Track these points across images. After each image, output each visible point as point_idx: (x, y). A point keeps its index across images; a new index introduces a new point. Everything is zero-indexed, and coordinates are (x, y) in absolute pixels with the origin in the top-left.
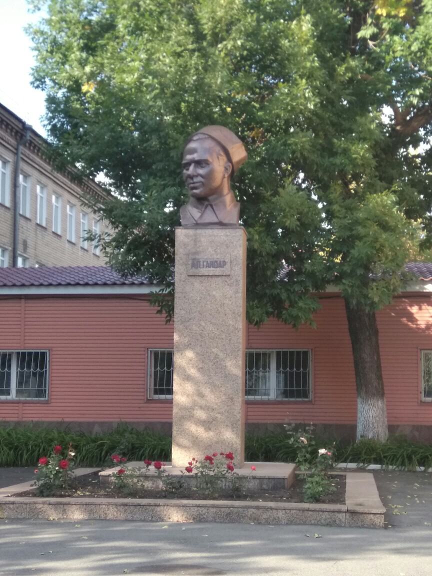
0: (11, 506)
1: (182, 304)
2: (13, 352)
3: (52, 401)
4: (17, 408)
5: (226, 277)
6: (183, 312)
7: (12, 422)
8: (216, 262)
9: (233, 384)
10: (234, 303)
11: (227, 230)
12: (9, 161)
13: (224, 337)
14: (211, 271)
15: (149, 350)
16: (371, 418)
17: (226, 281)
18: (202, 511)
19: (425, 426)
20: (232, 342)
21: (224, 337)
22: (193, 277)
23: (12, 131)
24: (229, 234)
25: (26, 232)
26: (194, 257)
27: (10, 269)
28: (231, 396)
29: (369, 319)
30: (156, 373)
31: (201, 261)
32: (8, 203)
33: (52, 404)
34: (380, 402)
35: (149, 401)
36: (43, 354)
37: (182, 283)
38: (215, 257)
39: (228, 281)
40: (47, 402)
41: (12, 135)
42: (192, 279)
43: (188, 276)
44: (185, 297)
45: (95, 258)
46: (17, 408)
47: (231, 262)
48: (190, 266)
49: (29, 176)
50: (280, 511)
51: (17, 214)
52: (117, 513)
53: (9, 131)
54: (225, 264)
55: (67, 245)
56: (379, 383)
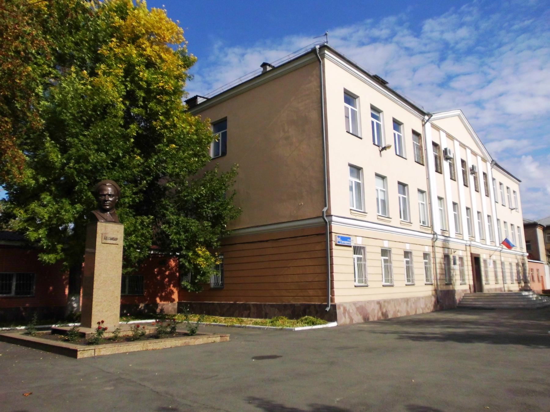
0: (104, 349)
14: (112, 242)
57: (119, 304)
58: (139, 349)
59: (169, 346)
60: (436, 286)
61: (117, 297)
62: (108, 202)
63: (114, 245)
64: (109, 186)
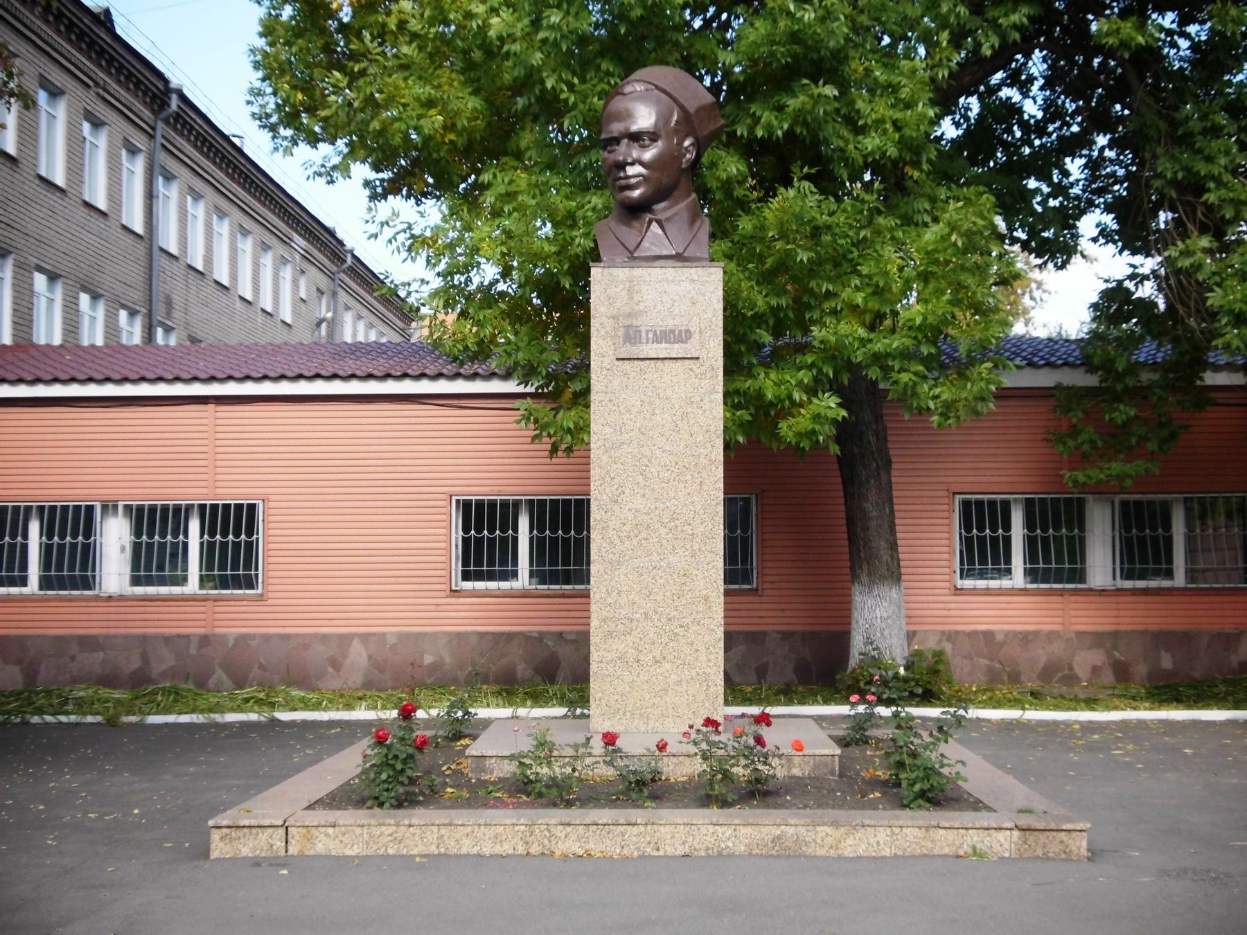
0: (330, 831)
2: (193, 505)
3: (270, 595)
4: (203, 609)
5: (692, 362)
6: (607, 430)
7: (195, 635)
8: (673, 331)
10: (708, 412)
11: (693, 270)
12: (141, 150)
14: (662, 350)
15: (454, 498)
16: (879, 621)
18: (724, 833)
19: (963, 632)
20: (705, 488)
21: (689, 477)
22: (627, 362)
23: (145, 94)
24: (695, 277)
25: (171, 282)
26: (628, 322)
27: (141, 348)
28: (704, 592)
29: (877, 439)
30: (466, 541)
31: (643, 329)
32: (139, 227)
33: (270, 602)
34: (894, 590)
35: (455, 593)
36: (252, 508)
37: (606, 372)
38: (670, 323)
40: (261, 598)
41: (145, 103)
42: (627, 365)
44: (610, 401)
45: (285, 329)
46: (203, 609)
47: (701, 332)
48: (621, 340)
49: (174, 177)
50: (881, 829)
51: (155, 249)
52: (550, 841)
53: (140, 94)
54: (690, 338)
55: (239, 304)
56: (892, 557)
57: (720, 633)
58: (507, 848)
59: (680, 851)
60: (1210, 522)
61: (706, 598)
62: (631, 170)
63: (679, 363)
64: (642, 98)
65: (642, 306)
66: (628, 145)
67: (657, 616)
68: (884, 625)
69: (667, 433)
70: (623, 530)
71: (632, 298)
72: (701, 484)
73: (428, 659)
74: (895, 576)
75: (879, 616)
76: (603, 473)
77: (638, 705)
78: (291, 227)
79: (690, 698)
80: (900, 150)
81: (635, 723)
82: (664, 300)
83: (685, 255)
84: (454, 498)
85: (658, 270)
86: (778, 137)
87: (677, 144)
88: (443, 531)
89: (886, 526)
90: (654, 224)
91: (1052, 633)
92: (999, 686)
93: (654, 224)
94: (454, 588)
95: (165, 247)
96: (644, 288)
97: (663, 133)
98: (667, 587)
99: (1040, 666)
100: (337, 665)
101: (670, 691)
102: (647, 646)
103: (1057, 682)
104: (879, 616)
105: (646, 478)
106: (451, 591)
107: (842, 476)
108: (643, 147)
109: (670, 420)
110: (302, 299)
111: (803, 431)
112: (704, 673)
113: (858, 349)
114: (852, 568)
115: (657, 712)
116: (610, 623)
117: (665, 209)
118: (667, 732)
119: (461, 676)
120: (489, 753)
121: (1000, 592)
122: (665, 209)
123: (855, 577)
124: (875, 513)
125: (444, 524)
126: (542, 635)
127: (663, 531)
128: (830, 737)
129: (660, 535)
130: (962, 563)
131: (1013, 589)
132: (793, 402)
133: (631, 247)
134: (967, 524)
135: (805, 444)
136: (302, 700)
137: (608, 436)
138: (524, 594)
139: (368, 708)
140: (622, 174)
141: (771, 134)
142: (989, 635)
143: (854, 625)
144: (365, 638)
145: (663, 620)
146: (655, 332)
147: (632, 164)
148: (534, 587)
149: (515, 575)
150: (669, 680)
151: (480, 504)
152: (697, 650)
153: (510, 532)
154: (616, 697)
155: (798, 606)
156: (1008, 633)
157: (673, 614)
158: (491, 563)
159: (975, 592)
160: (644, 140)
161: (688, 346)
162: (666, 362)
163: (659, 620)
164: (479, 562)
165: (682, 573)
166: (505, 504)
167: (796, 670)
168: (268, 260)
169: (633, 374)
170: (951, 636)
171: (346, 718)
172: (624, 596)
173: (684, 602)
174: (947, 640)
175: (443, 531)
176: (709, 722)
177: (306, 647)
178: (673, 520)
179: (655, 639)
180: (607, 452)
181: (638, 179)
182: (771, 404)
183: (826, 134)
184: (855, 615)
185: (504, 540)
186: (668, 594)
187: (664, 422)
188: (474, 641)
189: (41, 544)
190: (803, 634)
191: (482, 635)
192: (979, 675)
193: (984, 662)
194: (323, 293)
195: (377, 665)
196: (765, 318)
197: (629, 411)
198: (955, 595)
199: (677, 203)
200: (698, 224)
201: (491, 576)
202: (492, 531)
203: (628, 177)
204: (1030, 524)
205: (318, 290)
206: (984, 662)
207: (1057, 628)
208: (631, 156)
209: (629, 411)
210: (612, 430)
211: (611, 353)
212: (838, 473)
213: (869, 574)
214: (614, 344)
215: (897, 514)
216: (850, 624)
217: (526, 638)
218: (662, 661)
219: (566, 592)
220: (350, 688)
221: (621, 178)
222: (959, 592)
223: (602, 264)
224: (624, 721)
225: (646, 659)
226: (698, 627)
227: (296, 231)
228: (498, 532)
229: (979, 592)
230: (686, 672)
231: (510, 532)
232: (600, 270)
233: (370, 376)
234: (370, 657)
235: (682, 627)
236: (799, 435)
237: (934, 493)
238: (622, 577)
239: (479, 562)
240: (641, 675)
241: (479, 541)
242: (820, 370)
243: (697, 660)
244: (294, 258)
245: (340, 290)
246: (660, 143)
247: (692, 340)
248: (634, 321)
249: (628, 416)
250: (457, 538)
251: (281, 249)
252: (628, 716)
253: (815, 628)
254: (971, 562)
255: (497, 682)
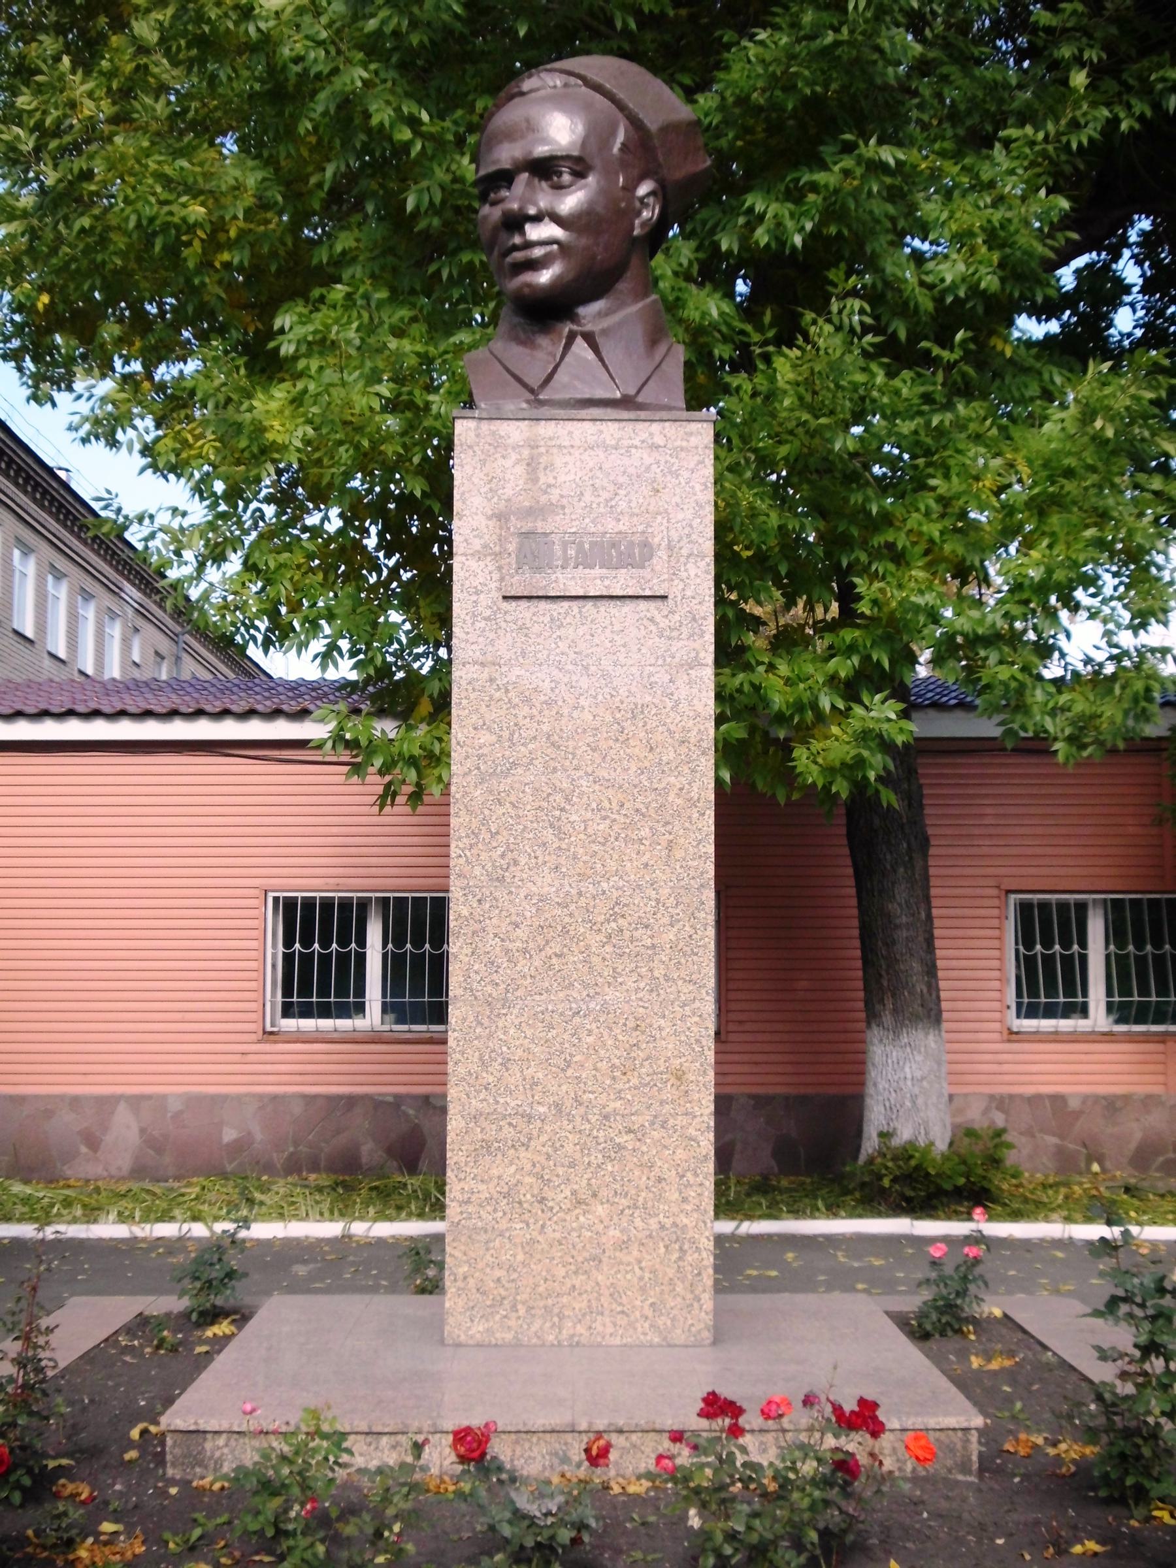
1: (483, 709)
5: (652, 605)
6: (485, 738)
9: (683, 1018)
11: (655, 427)
13: (645, 832)
15: (271, 895)
16: (909, 1083)
17: (652, 620)
19: (1021, 1097)
20: (679, 854)
21: (645, 832)
22: (524, 604)
24: (659, 440)
26: (527, 526)
30: (288, 959)
34: (931, 1037)
35: (270, 1035)
39: (658, 618)
43: (505, 598)
47: (670, 547)
48: (513, 559)
55: (47, 662)
56: (929, 986)
61: (680, 1075)
62: (534, 232)
63: (629, 606)
64: (560, 101)
65: (555, 494)
66: (529, 184)
67: (582, 1110)
68: (916, 1090)
69: (603, 745)
70: (513, 936)
71: (535, 480)
72: (670, 846)
73: (229, 1135)
74: (932, 1015)
75: (909, 1076)
76: (475, 824)
77: (541, 1289)
78: (121, 574)
79: (647, 1275)
80: (1003, 280)
81: (536, 1326)
82: (598, 483)
83: (640, 399)
84: (271, 895)
85: (587, 425)
86: (794, 247)
87: (624, 188)
88: (254, 944)
89: (921, 939)
90: (579, 340)
91: (1149, 1097)
92: (1078, 1178)
93: (579, 340)
94: (269, 1028)
95: (20, 630)
96: (559, 461)
97: (597, 162)
98: (602, 1052)
99: (1133, 1146)
100: (93, 1143)
101: (605, 1259)
102: (560, 1171)
103: (1157, 1170)
104: (909, 1076)
105: (560, 834)
106: (265, 1032)
107: (855, 866)
108: (559, 187)
109: (609, 718)
110: (135, 663)
111: (837, 764)
112: (675, 1224)
113: (925, 626)
114: (868, 1003)
115: (580, 1305)
116: (485, 1124)
117: (601, 315)
118: (599, 1345)
119: (278, 1159)
120: (212, 1425)
121: (1074, 1037)
122: (601, 315)
123: (872, 1016)
124: (904, 919)
125: (254, 933)
126: (399, 1099)
127: (594, 940)
128: (887, 1313)
129: (588, 947)
130: (1019, 994)
131: (1093, 1033)
132: (820, 717)
133: (534, 381)
134: (1026, 937)
135: (841, 788)
136: (26, 1200)
137: (485, 751)
138: (374, 1038)
139: (122, 1218)
140: (517, 240)
141: (782, 243)
142: (1058, 1100)
143: (870, 1090)
144: (136, 1102)
145: (593, 1119)
146: (581, 544)
147: (537, 219)
148: (386, 1027)
149: (360, 1009)
150: (604, 1239)
151: (309, 904)
152: (660, 1180)
153: (353, 945)
154: (498, 1273)
155: (773, 1058)
156: (1085, 1098)
157: (612, 1105)
158: (324, 991)
159: (1038, 1037)
160: (560, 174)
161: (646, 573)
162: (600, 603)
163: (585, 1118)
164: (305, 990)
165: (631, 1024)
166: (345, 904)
167: (776, 1154)
168: (89, 613)
169: (536, 629)
170: (1002, 1103)
171: (83, 1235)
172: (515, 1068)
173: (635, 1081)
174: (997, 1108)
175: (254, 944)
176: (715, 1405)
177: (49, 1114)
178: (614, 917)
179: (578, 1156)
180: (483, 781)
181: (548, 248)
182: (780, 718)
183: (876, 245)
184: (873, 1073)
185: (1067, 961)
186: (603, 1065)
187: (597, 723)
188: (297, 1109)
189: (1108, 957)
190: (787, 1098)
191: (310, 1099)
192: (1045, 1160)
193: (1052, 1140)
194: (163, 658)
195: (153, 1143)
196: (771, 563)
197: (527, 701)
198: (1009, 1041)
199: (622, 305)
200: (662, 349)
201: (325, 1011)
202: (325, 944)
203: (529, 245)
204: (1115, 933)
205: (157, 653)
206: (1052, 1140)
207: (1157, 1090)
208: (535, 204)
209: (527, 701)
210: (494, 738)
211: (493, 585)
212: (849, 862)
213: (895, 1011)
214: (500, 568)
215: (937, 923)
216: (863, 1084)
217: (375, 1104)
218: (590, 1200)
219: (435, 1035)
220: (112, 1177)
221: (516, 248)
222: (1014, 1037)
223: (477, 413)
224: (512, 1323)
225: (560, 1196)
226: (663, 1133)
227: (128, 580)
228: (334, 945)
229: (1043, 1037)
230: (638, 1222)
231: (353, 945)
232: (472, 424)
233: (147, 714)
234: (142, 1131)
235: (630, 1131)
236: (830, 771)
237: (979, 891)
238: (512, 1031)
239: (305, 990)
240: (548, 1230)
241: (307, 959)
242: (866, 659)
243: (659, 1198)
244: (125, 613)
245: (185, 656)
246: (591, 179)
247: (654, 561)
248: (539, 524)
249: (526, 710)
250: (274, 956)
251: (107, 600)
252: (522, 1310)
253: (803, 1090)
254: (1033, 993)
255: (331, 1169)
